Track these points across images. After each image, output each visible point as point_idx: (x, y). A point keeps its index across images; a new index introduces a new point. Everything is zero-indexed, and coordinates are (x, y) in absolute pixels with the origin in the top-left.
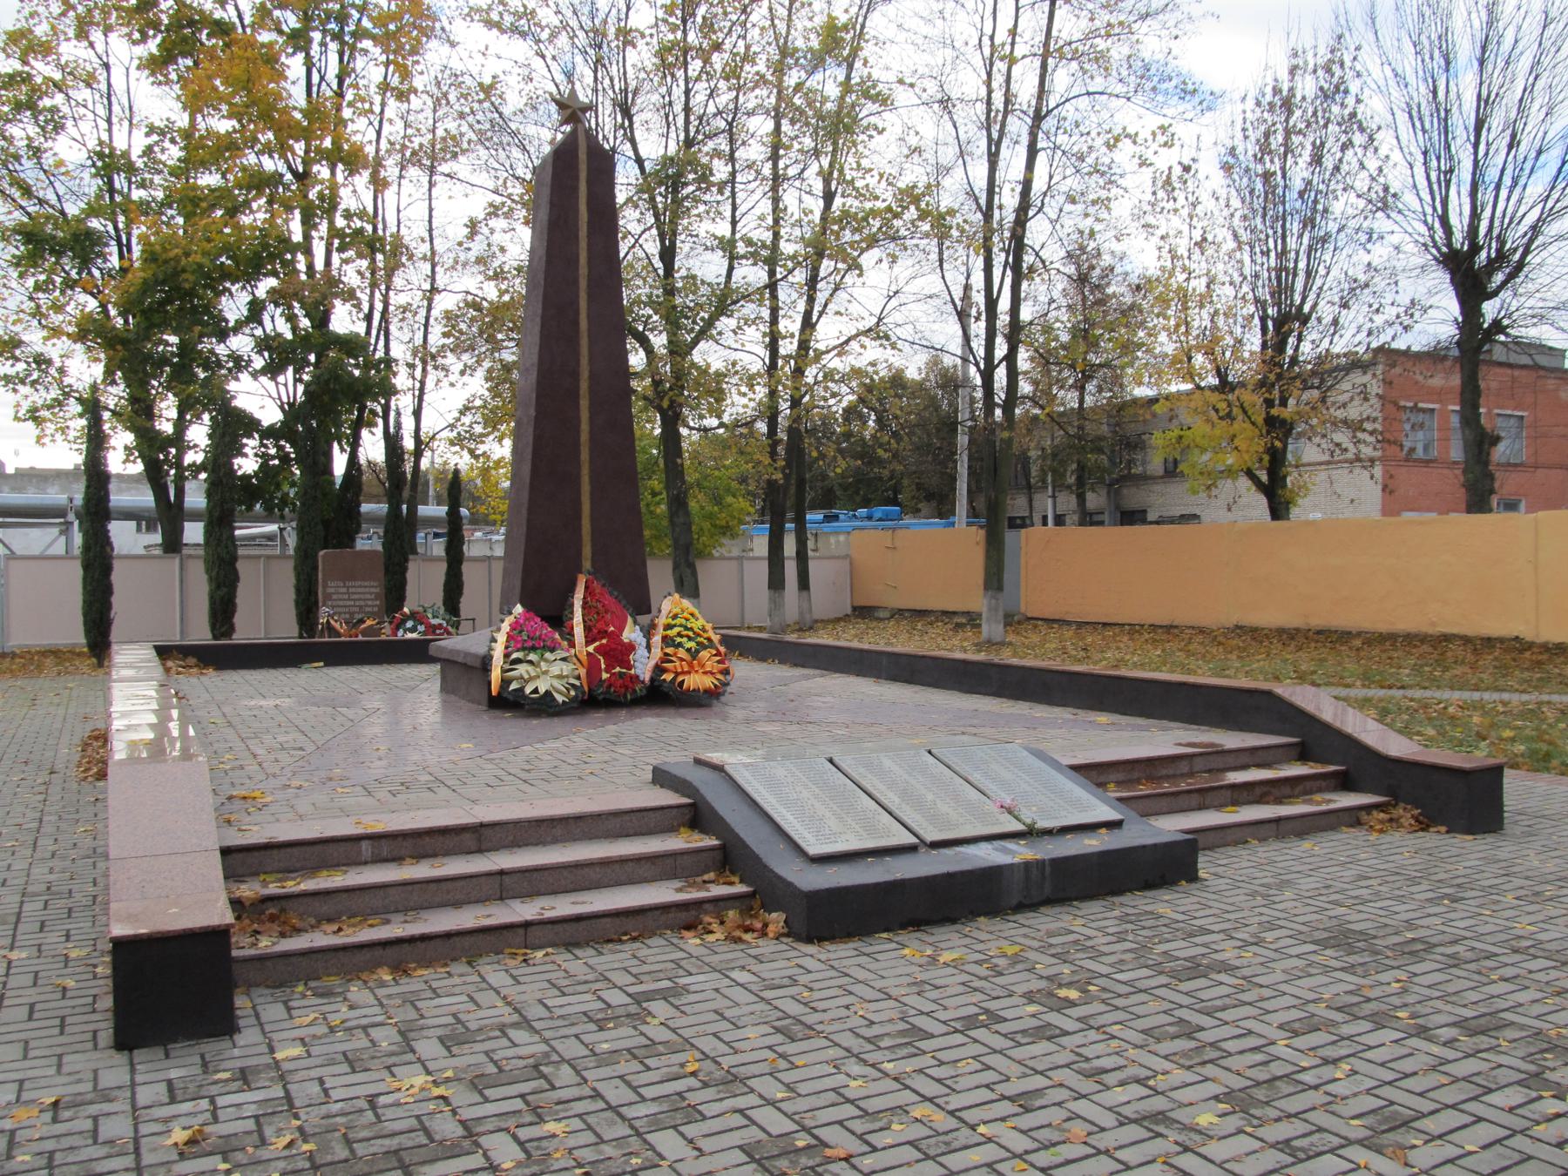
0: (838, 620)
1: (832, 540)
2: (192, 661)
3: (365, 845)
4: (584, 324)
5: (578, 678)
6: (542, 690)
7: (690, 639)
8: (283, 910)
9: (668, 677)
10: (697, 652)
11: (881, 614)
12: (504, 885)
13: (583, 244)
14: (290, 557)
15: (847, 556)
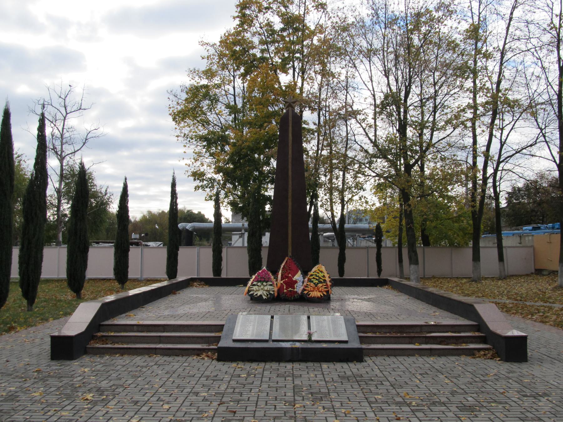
0: (527, 275)
1: (527, 239)
2: (203, 283)
3: (135, 327)
4: (290, 173)
5: (274, 291)
6: (258, 295)
7: (317, 279)
8: (107, 340)
9: (306, 292)
10: (318, 284)
11: (545, 273)
12: (161, 340)
13: (290, 147)
14: (245, 247)
15: (532, 246)
